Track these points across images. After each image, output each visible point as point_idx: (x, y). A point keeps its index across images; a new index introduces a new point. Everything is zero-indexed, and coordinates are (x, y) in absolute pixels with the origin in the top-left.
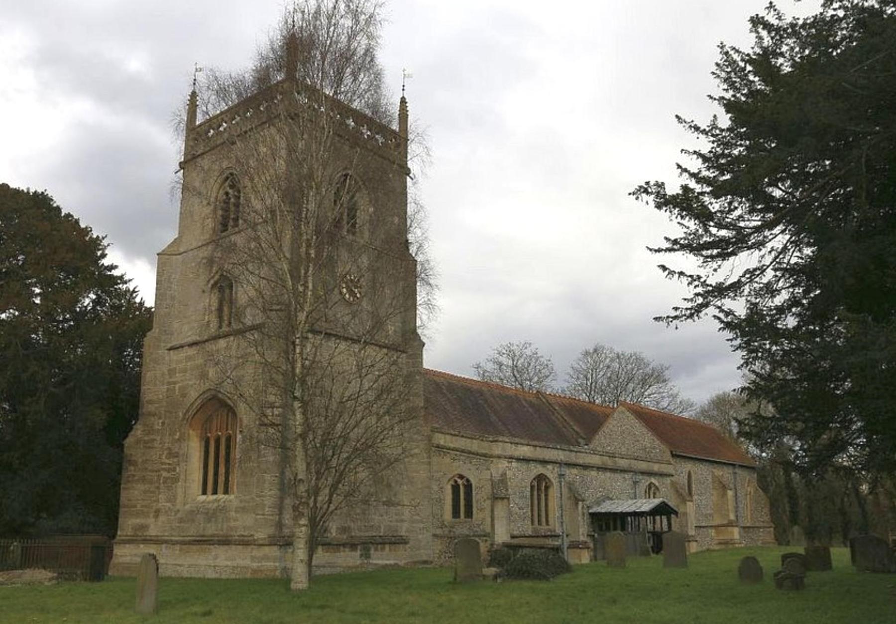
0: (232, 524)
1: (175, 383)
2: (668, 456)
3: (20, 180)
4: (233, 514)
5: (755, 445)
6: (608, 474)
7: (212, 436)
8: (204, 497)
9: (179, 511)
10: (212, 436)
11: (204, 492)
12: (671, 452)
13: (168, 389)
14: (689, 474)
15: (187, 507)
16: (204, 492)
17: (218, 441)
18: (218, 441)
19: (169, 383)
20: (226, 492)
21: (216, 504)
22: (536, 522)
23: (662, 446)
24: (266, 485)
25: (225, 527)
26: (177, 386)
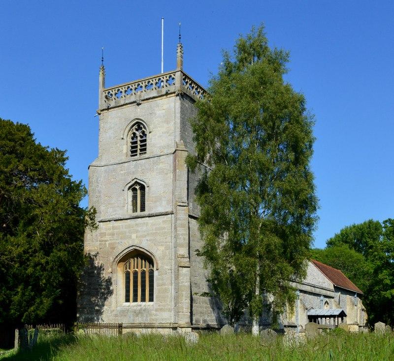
0: (154, 317)
1: (106, 241)
2: (332, 288)
3: (5, 117)
4: (154, 312)
5: (255, 293)
6: (312, 296)
7: (131, 271)
8: (128, 304)
9: (114, 311)
10: (131, 271)
11: (127, 300)
12: (334, 285)
13: (100, 244)
14: (333, 298)
15: (119, 308)
16: (127, 300)
17: (143, 277)
18: (143, 277)
19: (100, 241)
20: (151, 300)
21: (139, 308)
22: (128, 268)
23: (329, 281)
24: (184, 297)
25: (148, 319)
26: (107, 243)
